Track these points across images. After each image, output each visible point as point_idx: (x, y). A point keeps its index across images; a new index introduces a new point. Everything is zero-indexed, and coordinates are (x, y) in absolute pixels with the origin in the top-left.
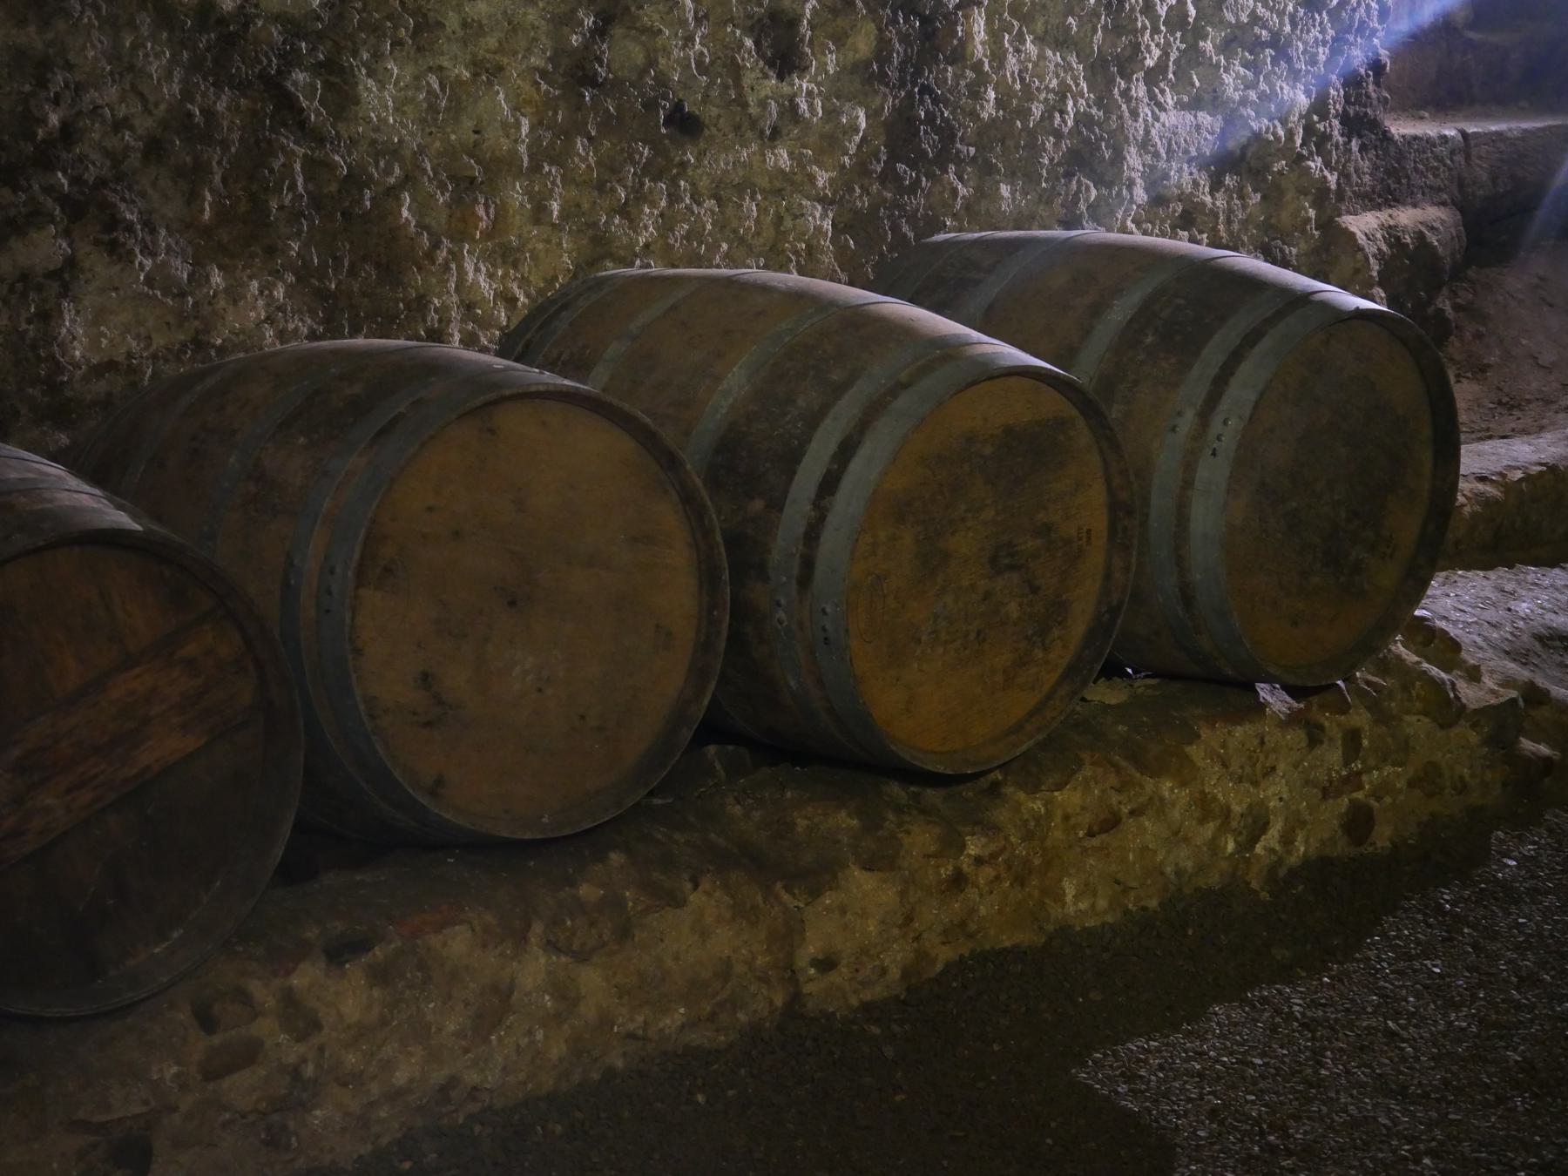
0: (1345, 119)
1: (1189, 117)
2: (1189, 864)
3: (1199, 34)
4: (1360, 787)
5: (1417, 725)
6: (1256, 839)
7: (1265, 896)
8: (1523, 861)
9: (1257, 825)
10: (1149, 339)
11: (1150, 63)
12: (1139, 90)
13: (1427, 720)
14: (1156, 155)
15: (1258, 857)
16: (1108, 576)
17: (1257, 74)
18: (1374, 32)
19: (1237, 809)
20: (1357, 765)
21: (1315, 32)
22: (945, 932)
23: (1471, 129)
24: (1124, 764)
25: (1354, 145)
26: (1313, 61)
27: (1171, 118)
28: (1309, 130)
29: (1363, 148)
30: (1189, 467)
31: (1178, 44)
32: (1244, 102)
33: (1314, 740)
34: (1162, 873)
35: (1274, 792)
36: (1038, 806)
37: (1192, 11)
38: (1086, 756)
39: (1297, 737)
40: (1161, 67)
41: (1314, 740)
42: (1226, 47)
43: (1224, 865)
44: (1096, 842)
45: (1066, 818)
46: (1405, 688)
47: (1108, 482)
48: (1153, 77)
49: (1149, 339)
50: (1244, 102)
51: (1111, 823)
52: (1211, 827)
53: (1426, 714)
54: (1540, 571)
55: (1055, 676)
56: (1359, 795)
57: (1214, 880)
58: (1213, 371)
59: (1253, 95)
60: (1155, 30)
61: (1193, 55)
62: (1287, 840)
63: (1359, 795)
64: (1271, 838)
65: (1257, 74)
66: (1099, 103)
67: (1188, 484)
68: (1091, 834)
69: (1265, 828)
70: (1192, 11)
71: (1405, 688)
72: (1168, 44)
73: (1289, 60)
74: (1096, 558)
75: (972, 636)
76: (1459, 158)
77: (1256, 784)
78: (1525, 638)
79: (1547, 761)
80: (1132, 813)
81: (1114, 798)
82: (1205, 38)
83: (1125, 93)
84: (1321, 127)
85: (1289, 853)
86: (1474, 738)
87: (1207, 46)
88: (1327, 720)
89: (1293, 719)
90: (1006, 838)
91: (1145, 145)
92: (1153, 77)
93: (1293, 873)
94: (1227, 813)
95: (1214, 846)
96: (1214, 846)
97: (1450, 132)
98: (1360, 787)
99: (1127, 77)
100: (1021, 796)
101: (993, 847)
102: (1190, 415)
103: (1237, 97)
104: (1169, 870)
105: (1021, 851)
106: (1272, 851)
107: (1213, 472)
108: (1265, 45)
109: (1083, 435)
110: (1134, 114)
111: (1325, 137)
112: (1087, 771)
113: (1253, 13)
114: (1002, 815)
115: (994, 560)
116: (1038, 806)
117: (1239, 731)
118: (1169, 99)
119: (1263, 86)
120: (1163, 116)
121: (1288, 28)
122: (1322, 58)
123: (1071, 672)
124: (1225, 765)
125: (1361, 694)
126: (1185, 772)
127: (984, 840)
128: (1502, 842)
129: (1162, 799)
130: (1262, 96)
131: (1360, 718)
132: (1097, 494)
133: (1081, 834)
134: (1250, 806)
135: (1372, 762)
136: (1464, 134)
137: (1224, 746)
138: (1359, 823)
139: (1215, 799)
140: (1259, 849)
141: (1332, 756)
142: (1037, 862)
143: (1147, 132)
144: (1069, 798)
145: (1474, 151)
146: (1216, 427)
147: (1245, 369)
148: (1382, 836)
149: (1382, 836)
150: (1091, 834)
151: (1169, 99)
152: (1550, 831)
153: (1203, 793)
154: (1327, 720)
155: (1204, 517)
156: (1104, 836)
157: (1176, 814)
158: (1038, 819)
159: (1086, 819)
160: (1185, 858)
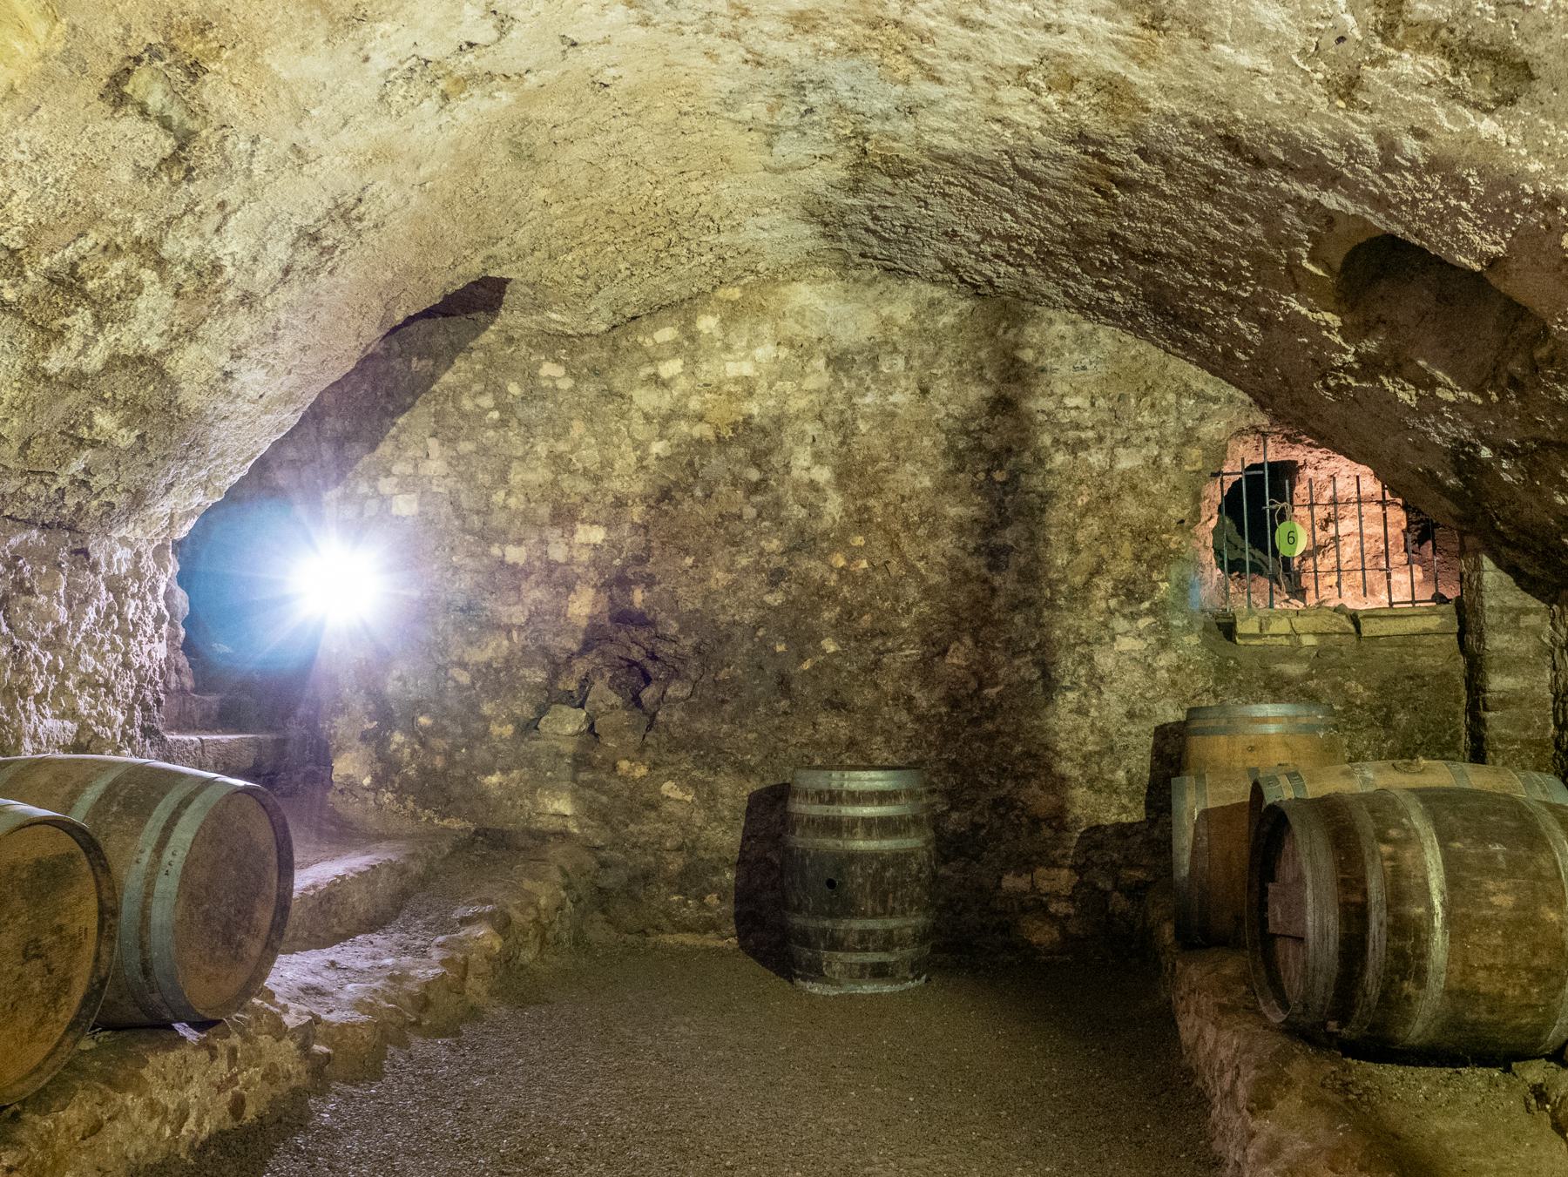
0: (143, 729)
1: (59, 723)
2: (143, 1149)
3: (65, 676)
4: (237, 1084)
5: (265, 1041)
6: (181, 1126)
7: (192, 1162)
8: (333, 1113)
9: (183, 1116)
10: (115, 809)
11: (38, 691)
12: (31, 706)
13: (270, 1037)
14: (40, 743)
15: (184, 1138)
16: (97, 959)
17: (97, 701)
18: (157, 683)
19: (172, 1107)
20: (235, 1070)
21: (127, 681)
22: (243, 1102)
23: (204, 738)
24: (102, 1087)
25: (148, 742)
26: (126, 696)
27: (50, 723)
28: (124, 733)
29: (152, 744)
30: (150, 883)
31: (53, 682)
32: (90, 716)
33: (213, 1058)
34: (127, 1158)
35: (193, 1091)
36: (49, 1123)
37: (62, 664)
38: (79, 1084)
39: (204, 1055)
40: (44, 694)
41: (213, 1058)
42: (81, 685)
43: (163, 1146)
44: (86, 1143)
45: (68, 1129)
46: (258, 1019)
47: (99, 893)
48: (39, 699)
49: (115, 809)
50: (90, 716)
51: (96, 1128)
52: (156, 1121)
53: (270, 1034)
54: (288, 956)
55: (61, 1032)
56: (237, 1088)
57: (158, 1157)
58: (161, 824)
59: (94, 713)
60: (41, 673)
61: (61, 689)
62: (199, 1123)
63: (237, 1088)
64: (190, 1124)
65: (97, 701)
66: (8, 712)
67: (149, 895)
68: (84, 1138)
69: (186, 1118)
70: (62, 664)
71: (258, 1019)
72: (48, 681)
73: (114, 695)
74: (90, 947)
75: (8, 1008)
76: (199, 752)
77: (181, 1089)
78: (295, 990)
79: (328, 1055)
80: (109, 1119)
81: (99, 1112)
82: (69, 679)
83: (23, 707)
84: (130, 732)
85: (201, 1131)
86: (292, 1045)
87: (69, 684)
88: (218, 1043)
89: (203, 1045)
90: (28, 1150)
91: (34, 737)
92: (39, 699)
93: (205, 1146)
94: (165, 1110)
95: (158, 1134)
96: (158, 1134)
97: (194, 738)
98: (237, 1084)
99: (24, 698)
100: (36, 1118)
101: (20, 1158)
102: (149, 851)
103: (86, 713)
104: (131, 1155)
105: (39, 1157)
106: (192, 1131)
107: (167, 885)
108: (100, 686)
109: (84, 865)
110: (28, 719)
111: (132, 738)
112: (80, 1095)
113: (95, 667)
114: (23, 1134)
115: (25, 954)
116: (49, 1123)
117: (172, 1056)
118: (48, 712)
119: (100, 708)
120: (45, 721)
121: (113, 678)
122: (131, 695)
123: (73, 1026)
124: (165, 1079)
125: (236, 1025)
126: (139, 1086)
127: (14, 1153)
128: (315, 1105)
129: (127, 1107)
130: (99, 713)
131: (235, 1040)
132: (92, 904)
133: (78, 1138)
134: (179, 1105)
135: (243, 1066)
136: (201, 740)
137: (164, 1066)
138: (237, 1106)
139: (159, 1102)
140: (184, 1132)
141: (222, 1065)
142: (49, 1163)
143: (36, 730)
144: (71, 1115)
145: (206, 749)
146: (167, 856)
147: (184, 821)
148: (250, 1113)
149: (250, 1113)
150: (84, 1138)
151: (48, 712)
152: (338, 1094)
153: (151, 1099)
154: (218, 1043)
155: (162, 914)
156: (93, 1138)
157: (135, 1116)
158: (49, 1133)
159: (81, 1128)
160: (140, 1145)
